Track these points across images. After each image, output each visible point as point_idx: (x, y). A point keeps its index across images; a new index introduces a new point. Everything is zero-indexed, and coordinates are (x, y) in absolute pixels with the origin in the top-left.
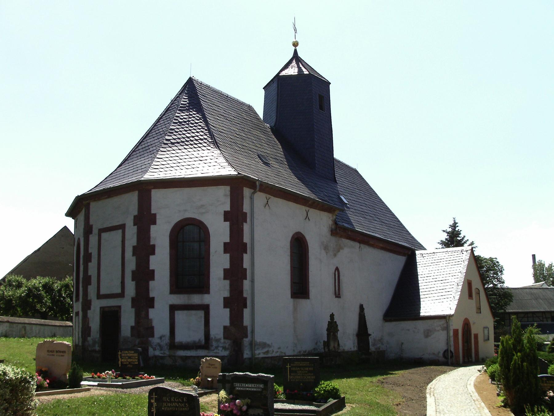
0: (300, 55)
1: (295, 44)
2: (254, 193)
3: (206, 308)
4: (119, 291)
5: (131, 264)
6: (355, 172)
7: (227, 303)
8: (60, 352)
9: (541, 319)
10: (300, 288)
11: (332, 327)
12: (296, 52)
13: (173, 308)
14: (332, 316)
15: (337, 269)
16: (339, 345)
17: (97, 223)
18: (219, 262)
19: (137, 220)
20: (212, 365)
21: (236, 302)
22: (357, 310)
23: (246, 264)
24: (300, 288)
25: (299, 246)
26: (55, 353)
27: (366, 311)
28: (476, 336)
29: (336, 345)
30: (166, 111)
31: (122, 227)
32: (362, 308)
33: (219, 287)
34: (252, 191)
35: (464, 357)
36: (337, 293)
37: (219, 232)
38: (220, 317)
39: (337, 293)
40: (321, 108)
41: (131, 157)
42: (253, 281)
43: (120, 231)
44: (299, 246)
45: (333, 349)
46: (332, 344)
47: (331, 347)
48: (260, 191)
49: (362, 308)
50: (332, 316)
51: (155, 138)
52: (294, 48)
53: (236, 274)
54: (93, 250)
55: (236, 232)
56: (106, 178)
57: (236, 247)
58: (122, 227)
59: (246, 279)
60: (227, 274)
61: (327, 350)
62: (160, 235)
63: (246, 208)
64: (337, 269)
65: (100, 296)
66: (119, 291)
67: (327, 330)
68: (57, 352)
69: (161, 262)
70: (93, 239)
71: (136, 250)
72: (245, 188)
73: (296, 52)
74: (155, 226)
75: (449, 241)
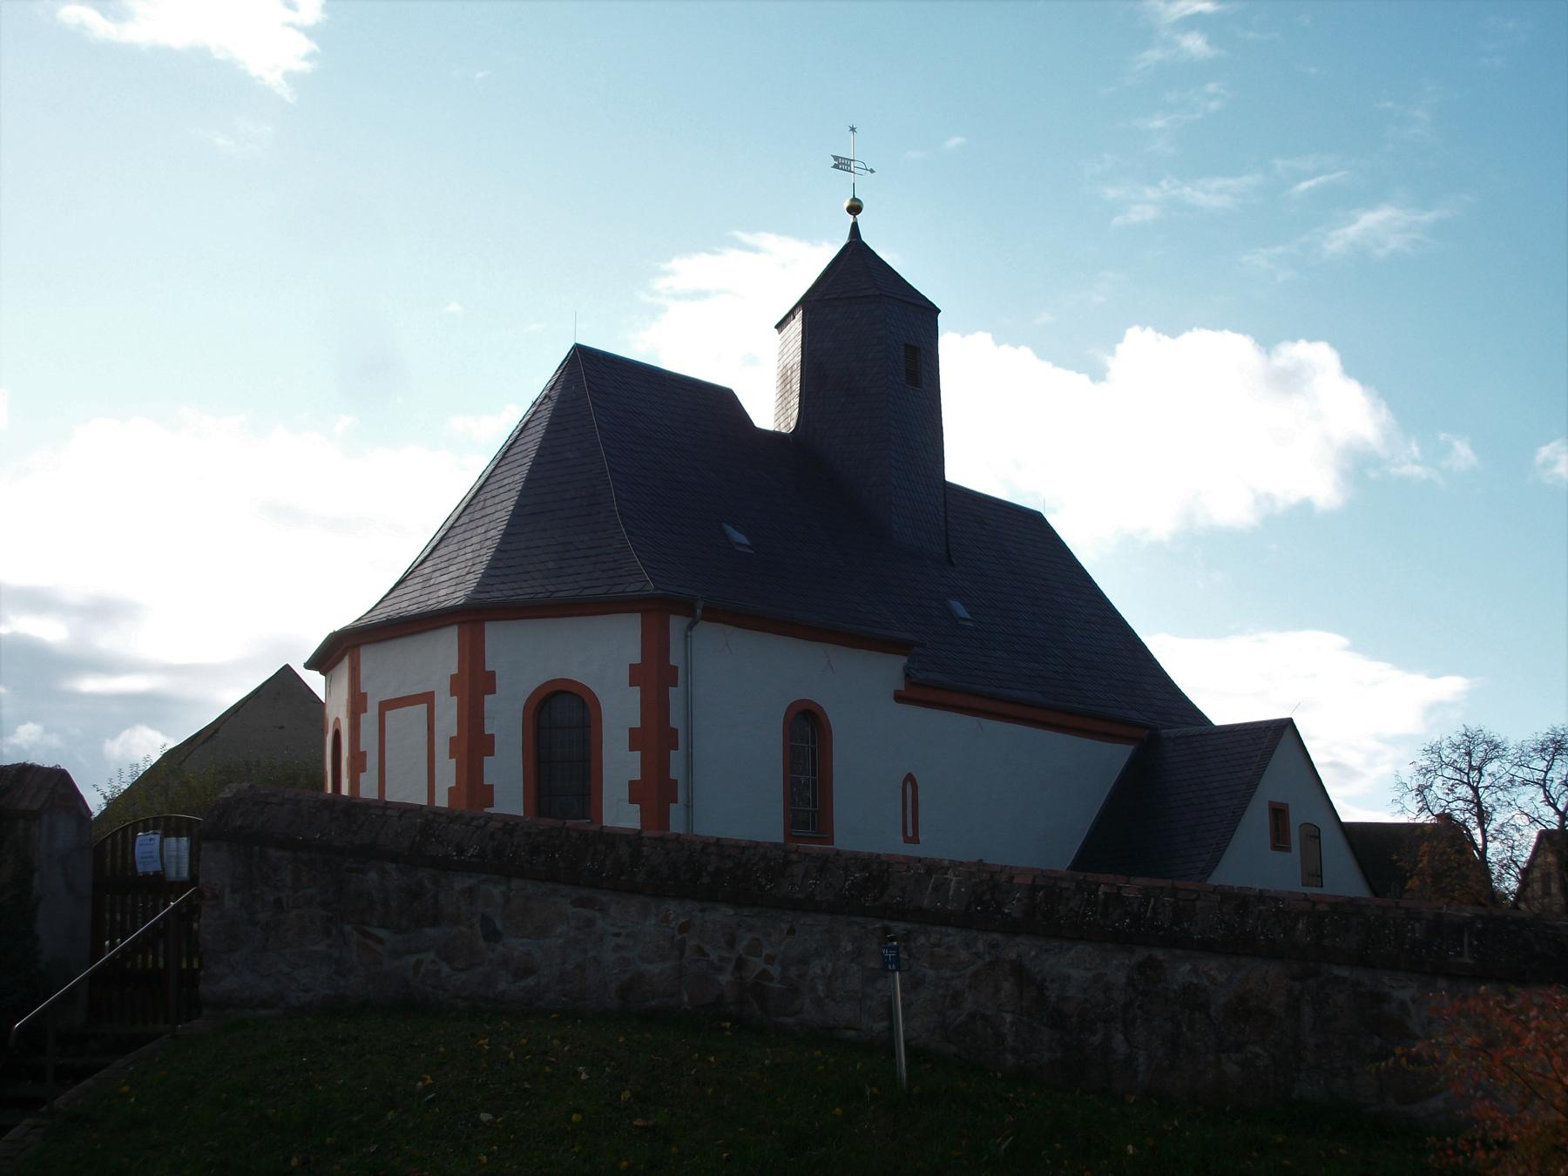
1: (855, 209)
2: (690, 627)
4: (389, 714)
12: (855, 229)
15: (910, 778)
19: (456, 685)
23: (676, 771)
25: (807, 730)
30: (522, 431)
34: (689, 620)
36: (910, 834)
37: (620, 710)
39: (910, 834)
42: (689, 806)
43: (422, 709)
44: (807, 730)
48: (704, 618)
51: (497, 500)
52: (851, 219)
54: (369, 743)
56: (392, 590)
57: (656, 738)
58: (427, 698)
59: (675, 801)
62: (505, 719)
63: (675, 658)
64: (910, 778)
66: (389, 714)
70: (369, 720)
73: (855, 229)
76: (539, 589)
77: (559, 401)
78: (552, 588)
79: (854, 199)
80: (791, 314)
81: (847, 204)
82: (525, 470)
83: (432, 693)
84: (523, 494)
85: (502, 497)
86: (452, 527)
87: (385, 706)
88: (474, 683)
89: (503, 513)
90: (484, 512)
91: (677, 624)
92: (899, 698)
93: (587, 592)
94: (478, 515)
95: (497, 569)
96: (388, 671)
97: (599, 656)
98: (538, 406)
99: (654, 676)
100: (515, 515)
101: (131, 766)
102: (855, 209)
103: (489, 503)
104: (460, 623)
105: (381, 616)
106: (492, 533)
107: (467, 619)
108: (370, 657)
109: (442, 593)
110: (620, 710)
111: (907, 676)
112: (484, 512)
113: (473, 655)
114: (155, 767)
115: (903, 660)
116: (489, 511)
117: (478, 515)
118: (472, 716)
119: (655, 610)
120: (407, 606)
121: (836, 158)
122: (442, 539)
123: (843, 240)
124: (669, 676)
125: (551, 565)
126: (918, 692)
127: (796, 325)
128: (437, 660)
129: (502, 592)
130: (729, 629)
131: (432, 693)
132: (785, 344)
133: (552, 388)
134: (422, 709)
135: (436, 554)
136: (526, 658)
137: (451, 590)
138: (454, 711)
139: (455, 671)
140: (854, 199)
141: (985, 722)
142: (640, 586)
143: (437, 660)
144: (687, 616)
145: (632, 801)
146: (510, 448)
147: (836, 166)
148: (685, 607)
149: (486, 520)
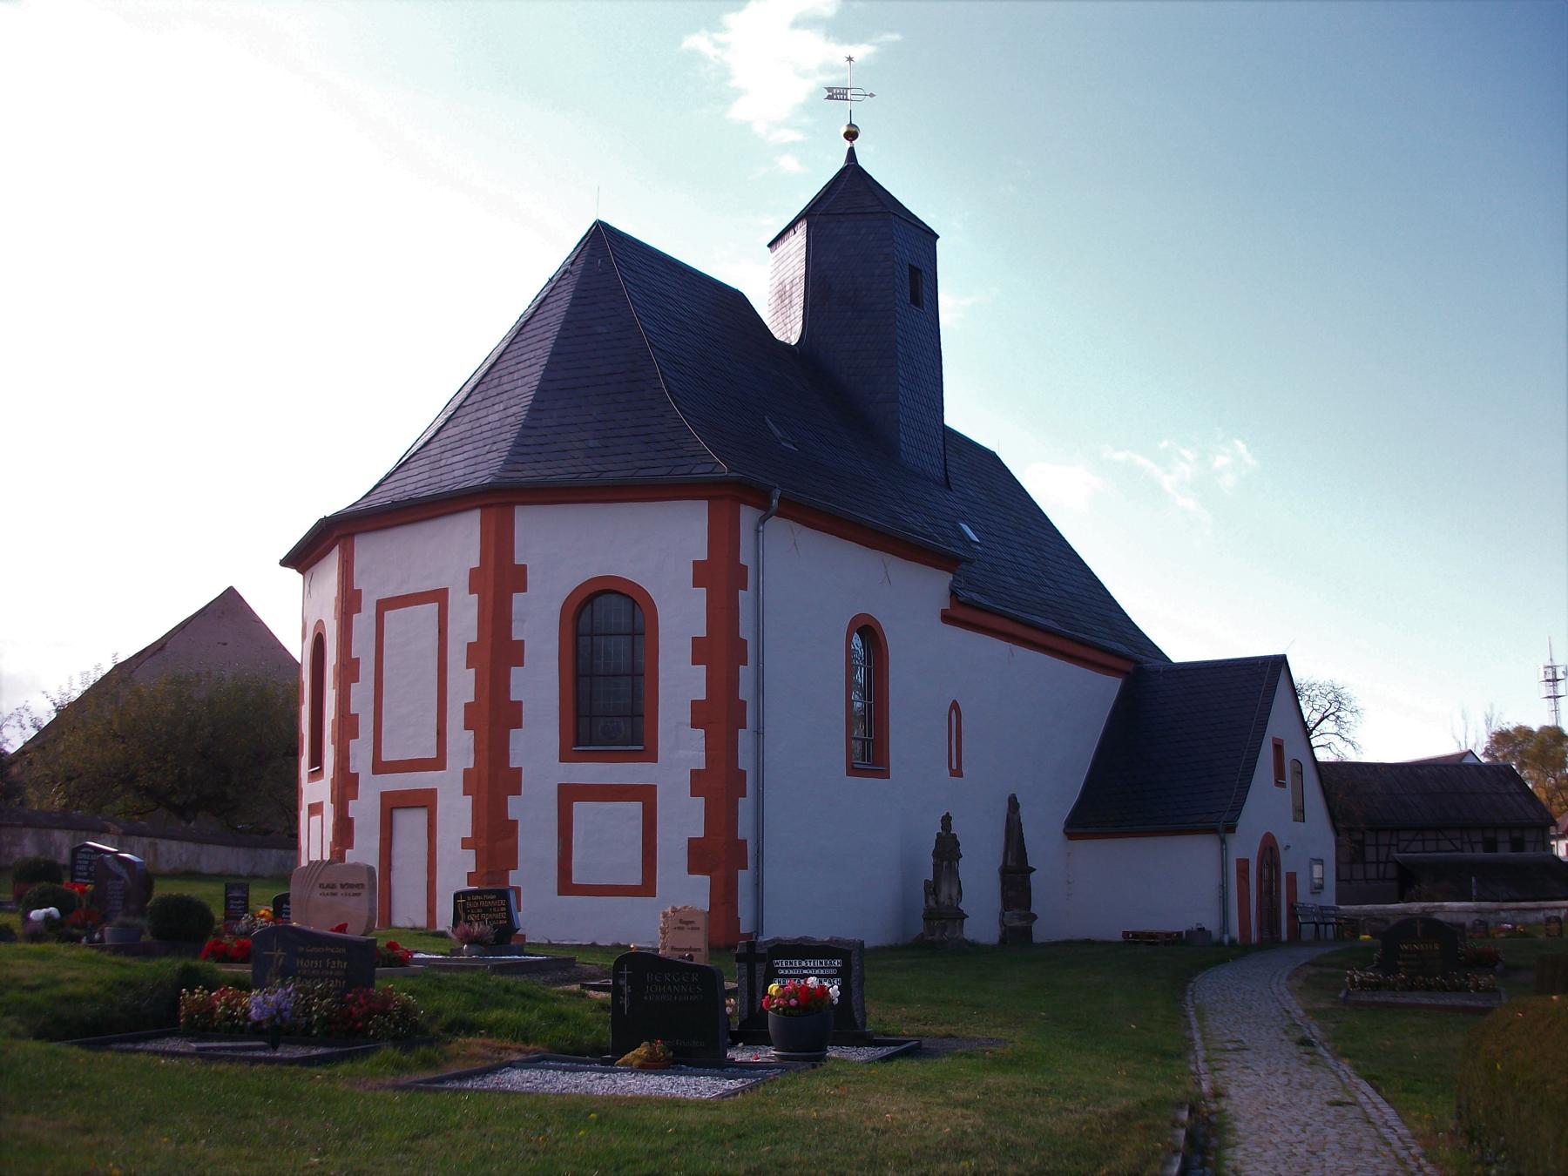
0: (863, 162)
1: (851, 135)
2: (763, 520)
3: (645, 795)
4: (389, 615)
5: (463, 685)
6: (992, 458)
7: (699, 783)
8: (351, 886)
9: (1458, 843)
10: (869, 752)
11: (947, 849)
13: (569, 795)
14: (946, 820)
15: (955, 706)
16: (960, 892)
17: (371, 590)
18: (680, 681)
19: (476, 581)
20: (687, 923)
21: (721, 783)
22: (1003, 807)
24: (869, 752)
26: (338, 890)
27: (1024, 813)
28: (1292, 878)
29: (955, 892)
30: (539, 307)
31: (439, 597)
32: (1013, 803)
33: (681, 747)
35: (1260, 930)
37: (681, 615)
38: (684, 818)
40: (916, 299)
41: (455, 422)
42: (759, 732)
45: (947, 902)
46: (945, 889)
47: (943, 897)
48: (779, 514)
49: (1013, 803)
50: (946, 820)
51: (516, 376)
52: (848, 145)
53: (721, 716)
54: (363, 648)
55: (723, 613)
57: (722, 650)
58: (439, 597)
60: (700, 715)
61: (932, 903)
62: (538, 622)
63: (746, 557)
64: (955, 706)
65: (380, 767)
66: (389, 615)
67: (935, 854)
68: (342, 886)
69: (538, 685)
70: (363, 622)
71: (473, 654)
72: (743, 508)
74: (1300, 672)
75: (1530, 747)
76: (583, 469)
77: (582, 276)
78: (600, 468)
79: (851, 125)
80: (791, 226)
81: (844, 129)
82: (549, 344)
83: (446, 590)
84: (549, 368)
85: (523, 373)
86: (460, 406)
87: (384, 606)
88: (500, 579)
89: (525, 389)
90: (499, 390)
91: (748, 516)
92: (947, 618)
93: (642, 473)
94: (493, 392)
95: (532, 436)
96: (387, 563)
97: (656, 548)
98: (554, 285)
99: (722, 576)
100: (540, 390)
101: (82, 674)
102: (851, 135)
103: (505, 379)
104: (481, 507)
105: (376, 502)
106: (514, 409)
107: (495, 500)
108: (367, 549)
109: (456, 473)
110: (681, 615)
111: (953, 594)
112: (499, 390)
113: (498, 545)
114: (106, 678)
115: (948, 577)
116: (506, 387)
117: (493, 392)
118: (496, 618)
119: (725, 496)
120: (417, 485)
121: (829, 89)
122: (448, 420)
123: (840, 162)
124: (738, 577)
125: (592, 443)
126: (963, 612)
127: (798, 240)
128: (456, 547)
129: (528, 473)
130: (797, 527)
131: (446, 590)
132: (781, 261)
133: (572, 264)
134: (432, 608)
135: (442, 435)
136: (564, 549)
137: (461, 473)
138: (474, 611)
139: (476, 563)
140: (851, 125)
141: (1021, 652)
142: (710, 468)
143: (456, 547)
144: (759, 507)
145: (694, 725)
146: (525, 324)
147: (829, 98)
148: (760, 499)
149: (505, 396)
